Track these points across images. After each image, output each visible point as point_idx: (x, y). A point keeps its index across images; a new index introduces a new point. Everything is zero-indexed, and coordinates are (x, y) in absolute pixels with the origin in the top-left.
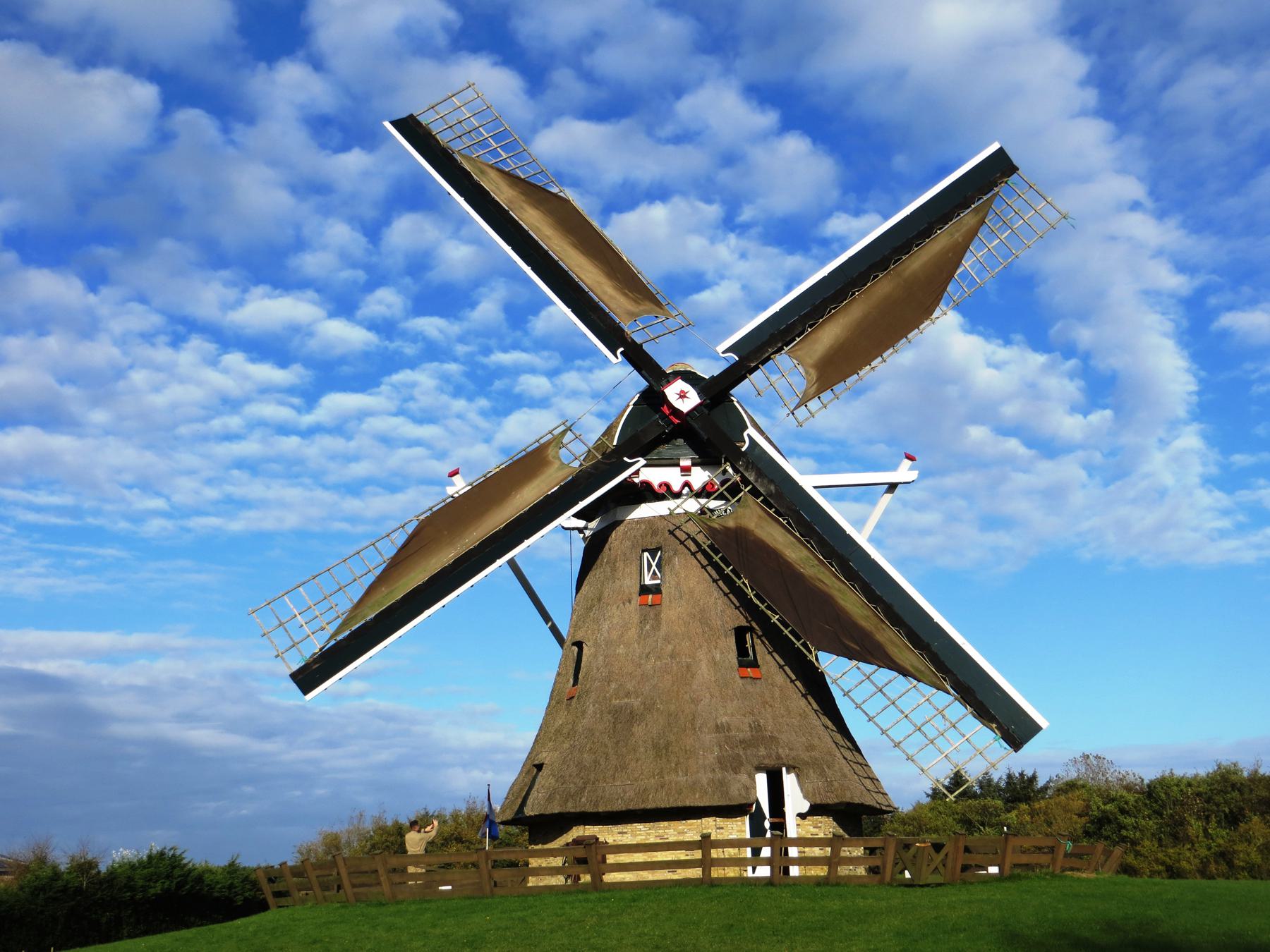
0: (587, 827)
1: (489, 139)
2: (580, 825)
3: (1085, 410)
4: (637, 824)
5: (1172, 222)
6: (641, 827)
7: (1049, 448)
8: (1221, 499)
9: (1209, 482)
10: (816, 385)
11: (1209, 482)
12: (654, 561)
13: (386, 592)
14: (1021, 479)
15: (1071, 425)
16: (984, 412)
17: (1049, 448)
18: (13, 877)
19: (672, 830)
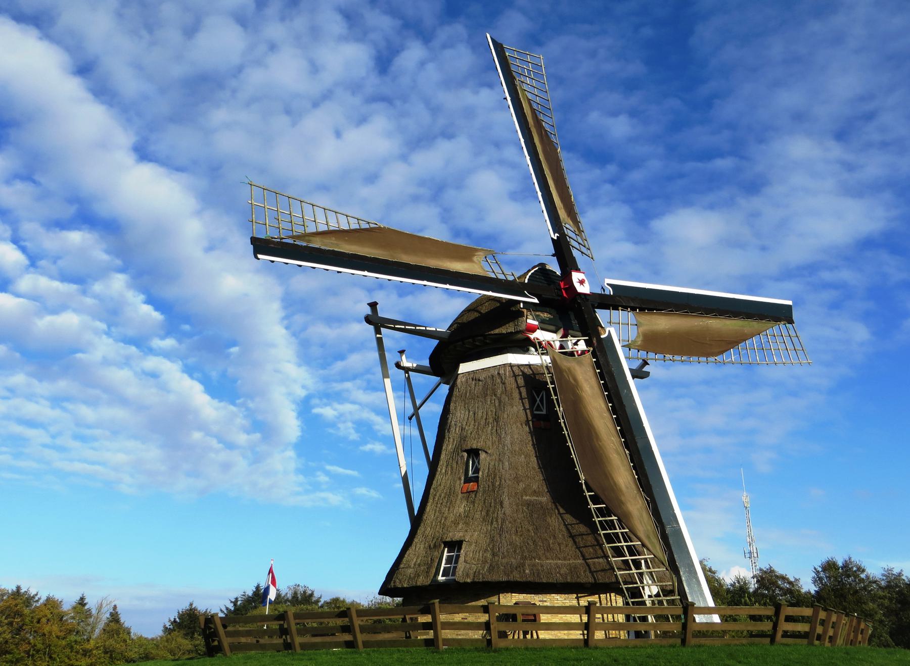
0: (513, 594)
1: (532, 72)
2: (507, 592)
3: (248, 432)
4: (554, 595)
5: (304, 368)
6: (558, 597)
7: (230, 446)
8: (301, 478)
9: (298, 471)
10: (476, 254)
11: (298, 471)
12: (538, 404)
13: (745, 329)
14: (212, 455)
15: (242, 438)
16: (203, 427)
17: (230, 446)
18: (210, 625)
19: (583, 602)
